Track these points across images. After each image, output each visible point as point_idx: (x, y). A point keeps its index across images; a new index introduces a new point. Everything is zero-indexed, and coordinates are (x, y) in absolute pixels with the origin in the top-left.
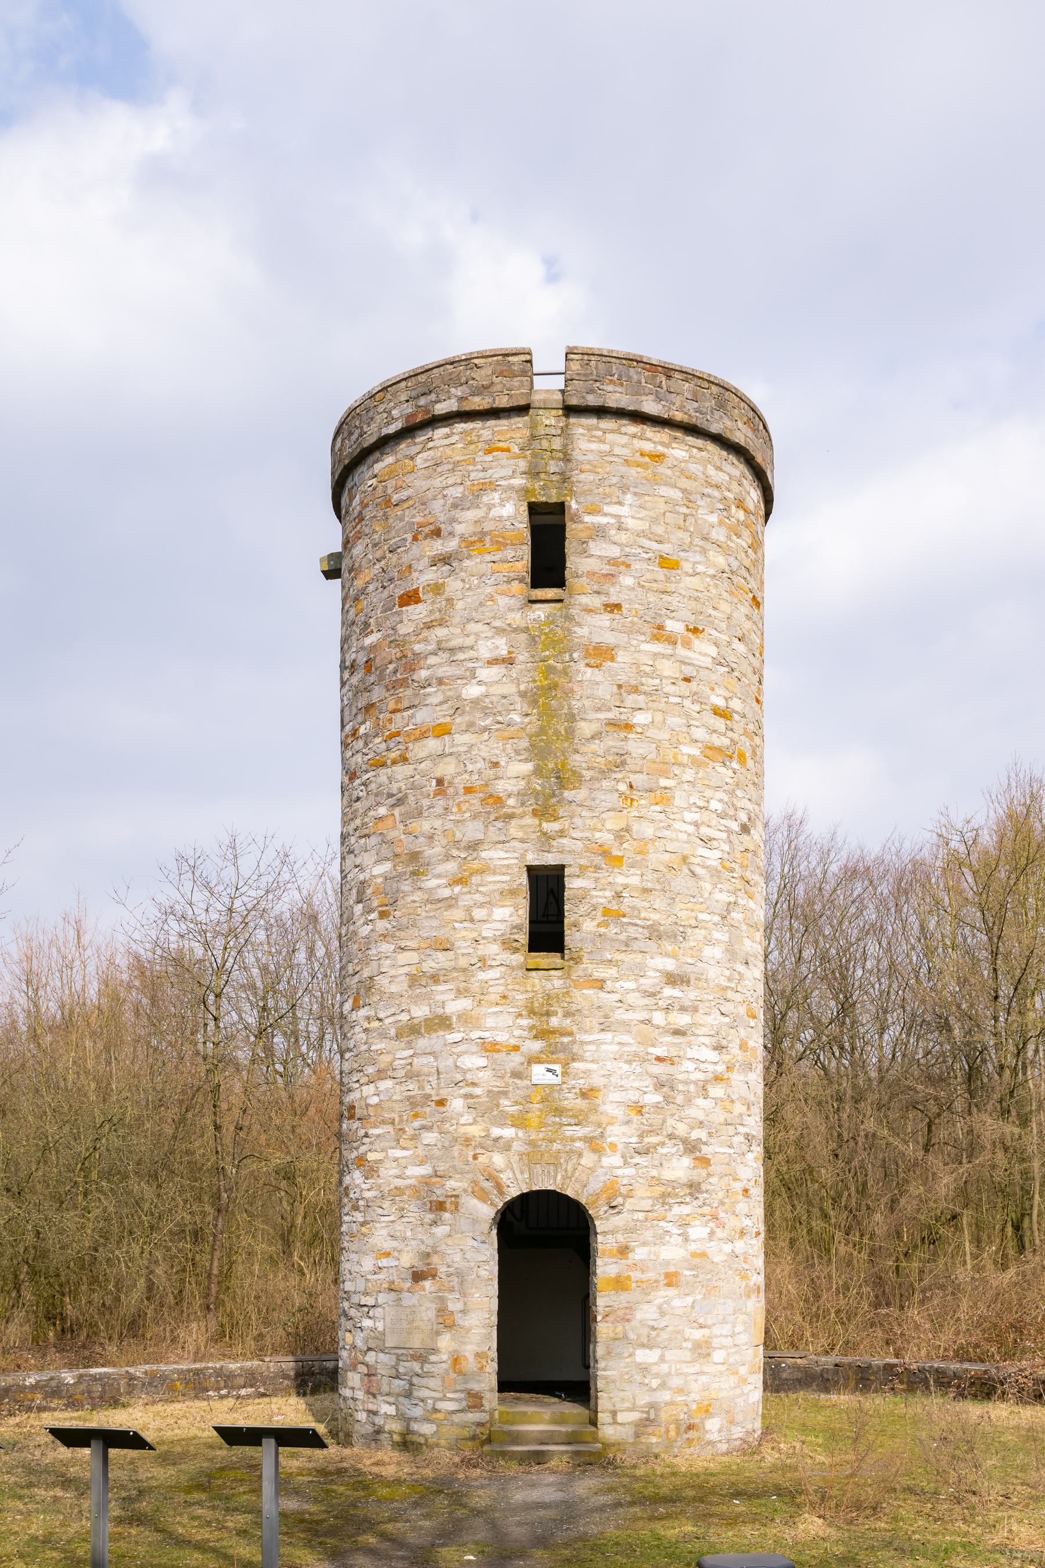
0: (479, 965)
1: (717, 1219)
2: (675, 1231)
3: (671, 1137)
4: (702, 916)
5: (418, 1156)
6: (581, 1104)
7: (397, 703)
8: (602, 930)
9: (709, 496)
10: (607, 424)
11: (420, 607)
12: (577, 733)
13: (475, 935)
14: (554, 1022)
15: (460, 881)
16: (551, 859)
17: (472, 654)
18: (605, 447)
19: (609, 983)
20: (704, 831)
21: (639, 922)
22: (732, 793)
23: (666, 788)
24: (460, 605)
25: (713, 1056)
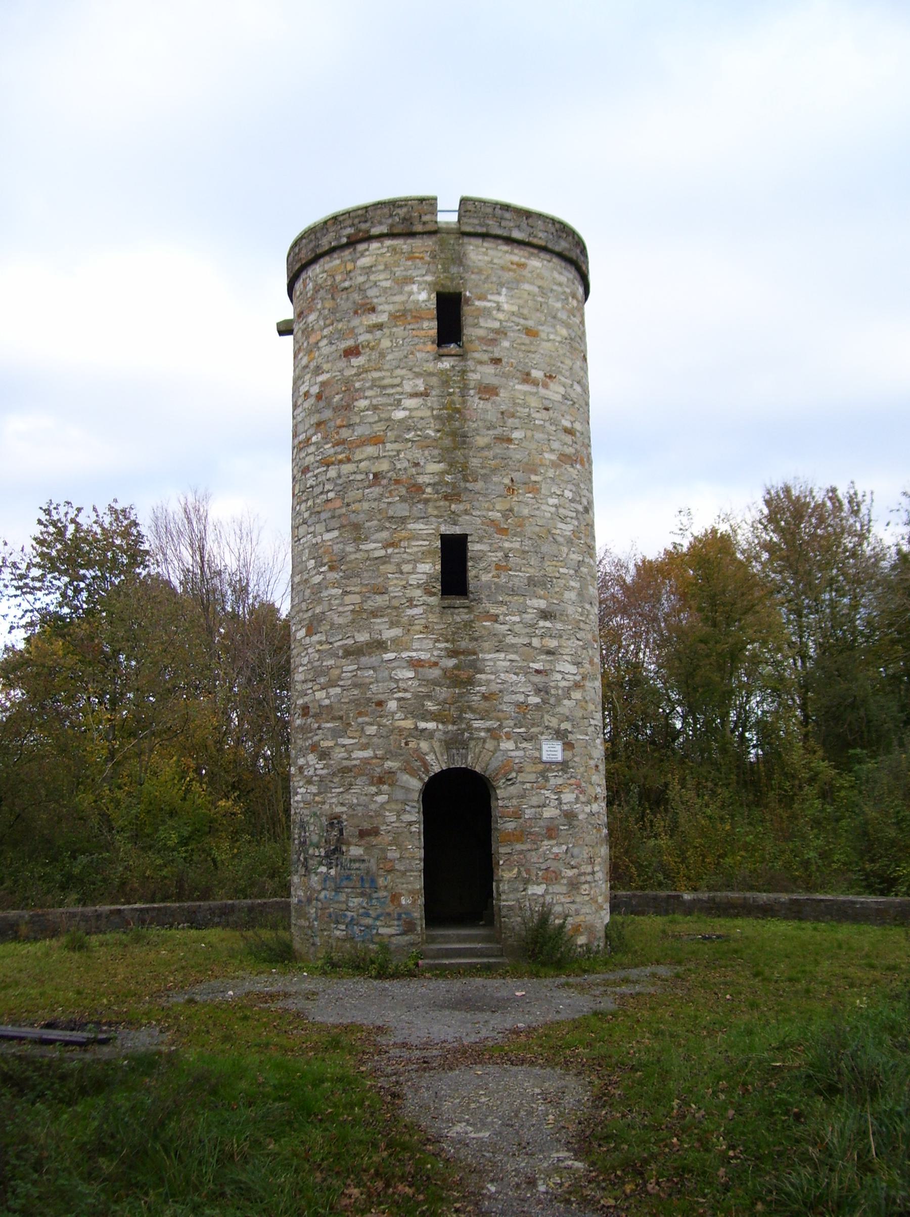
3: (547, 728)
4: (562, 570)
6: (485, 705)
13: (404, 582)
15: (392, 545)
16: (457, 530)
19: (501, 617)
25: (573, 669)
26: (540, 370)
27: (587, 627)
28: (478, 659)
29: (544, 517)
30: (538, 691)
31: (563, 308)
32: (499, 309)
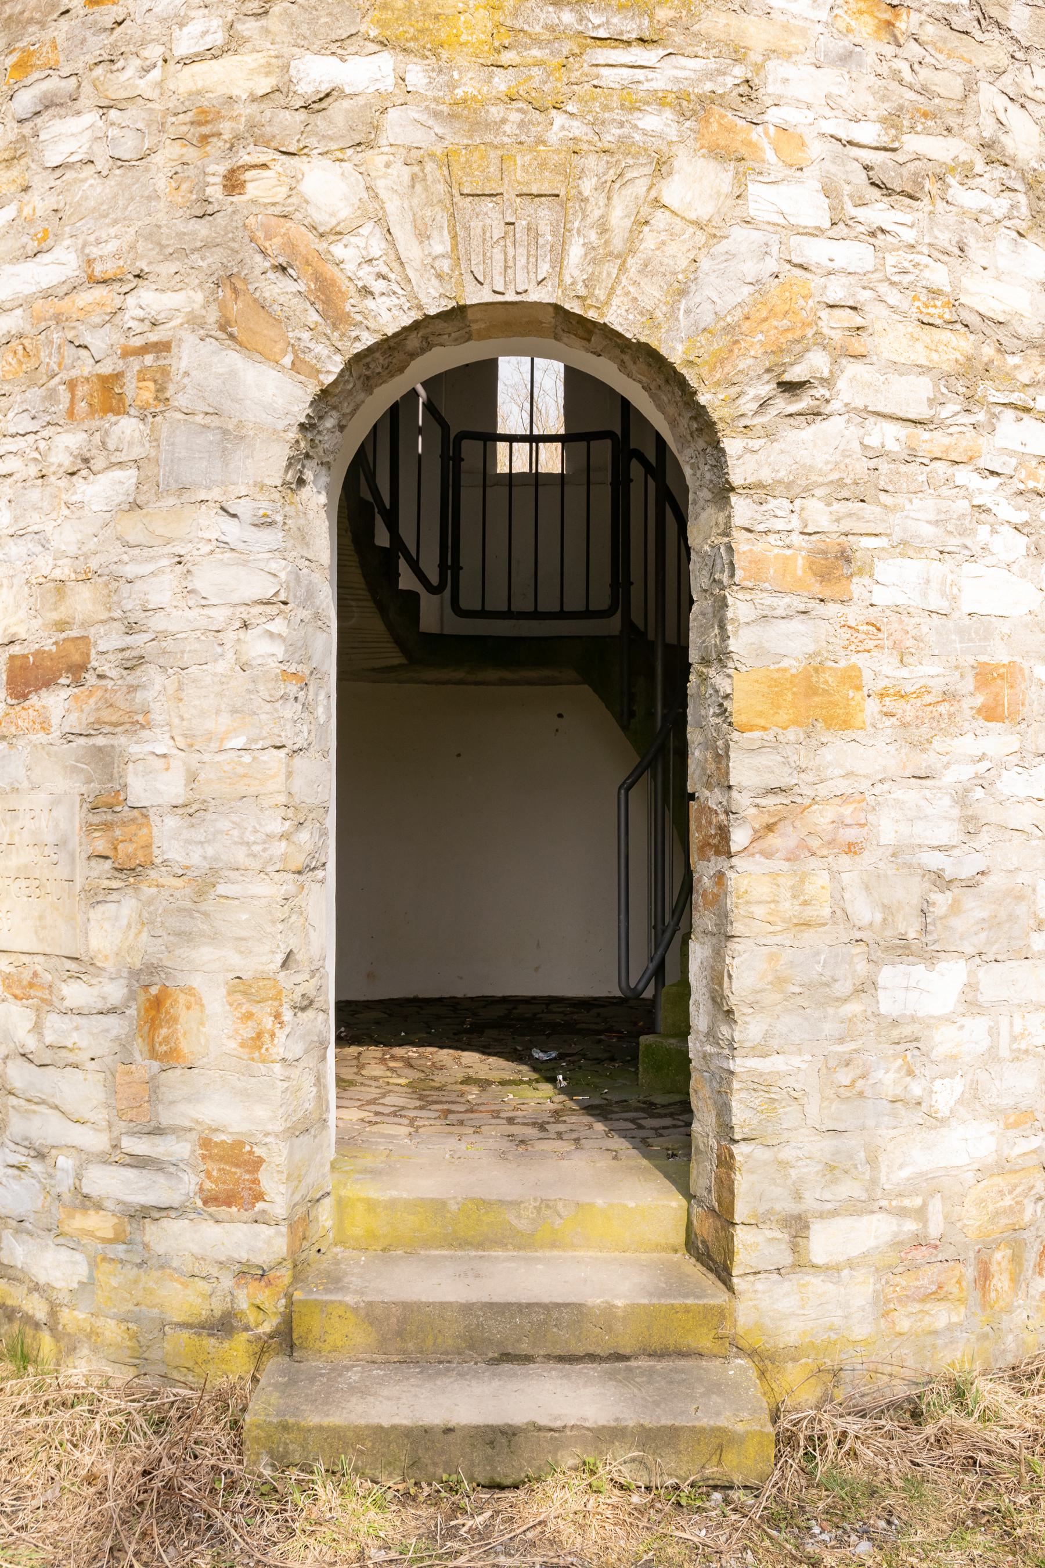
2: (1007, 511)
5: (30, 221)
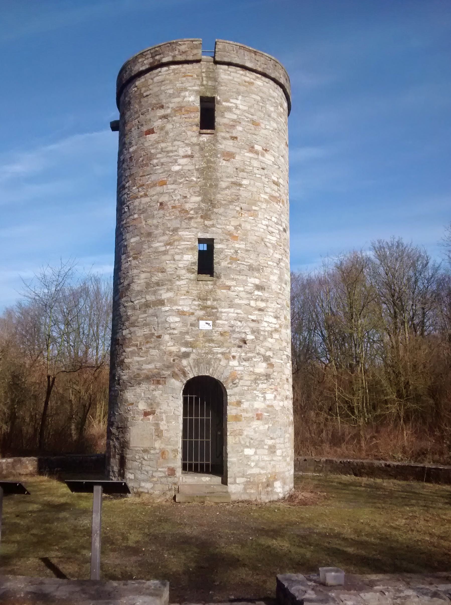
0: (177, 278)
1: (277, 391)
3: (258, 354)
4: (269, 263)
6: (221, 338)
7: (143, 173)
8: (230, 265)
9: (270, 100)
10: (232, 69)
11: (153, 135)
12: (219, 186)
13: (175, 266)
14: (209, 303)
15: (170, 244)
17: (176, 153)
18: (230, 78)
19: (232, 287)
20: (270, 228)
21: (245, 263)
22: (280, 215)
23: (255, 210)
24: (171, 134)
25: (274, 321)
26: (260, 145)
27: (283, 297)
28: (218, 312)
29: (260, 231)
30: (253, 332)
31: (275, 111)
32: (237, 108)
